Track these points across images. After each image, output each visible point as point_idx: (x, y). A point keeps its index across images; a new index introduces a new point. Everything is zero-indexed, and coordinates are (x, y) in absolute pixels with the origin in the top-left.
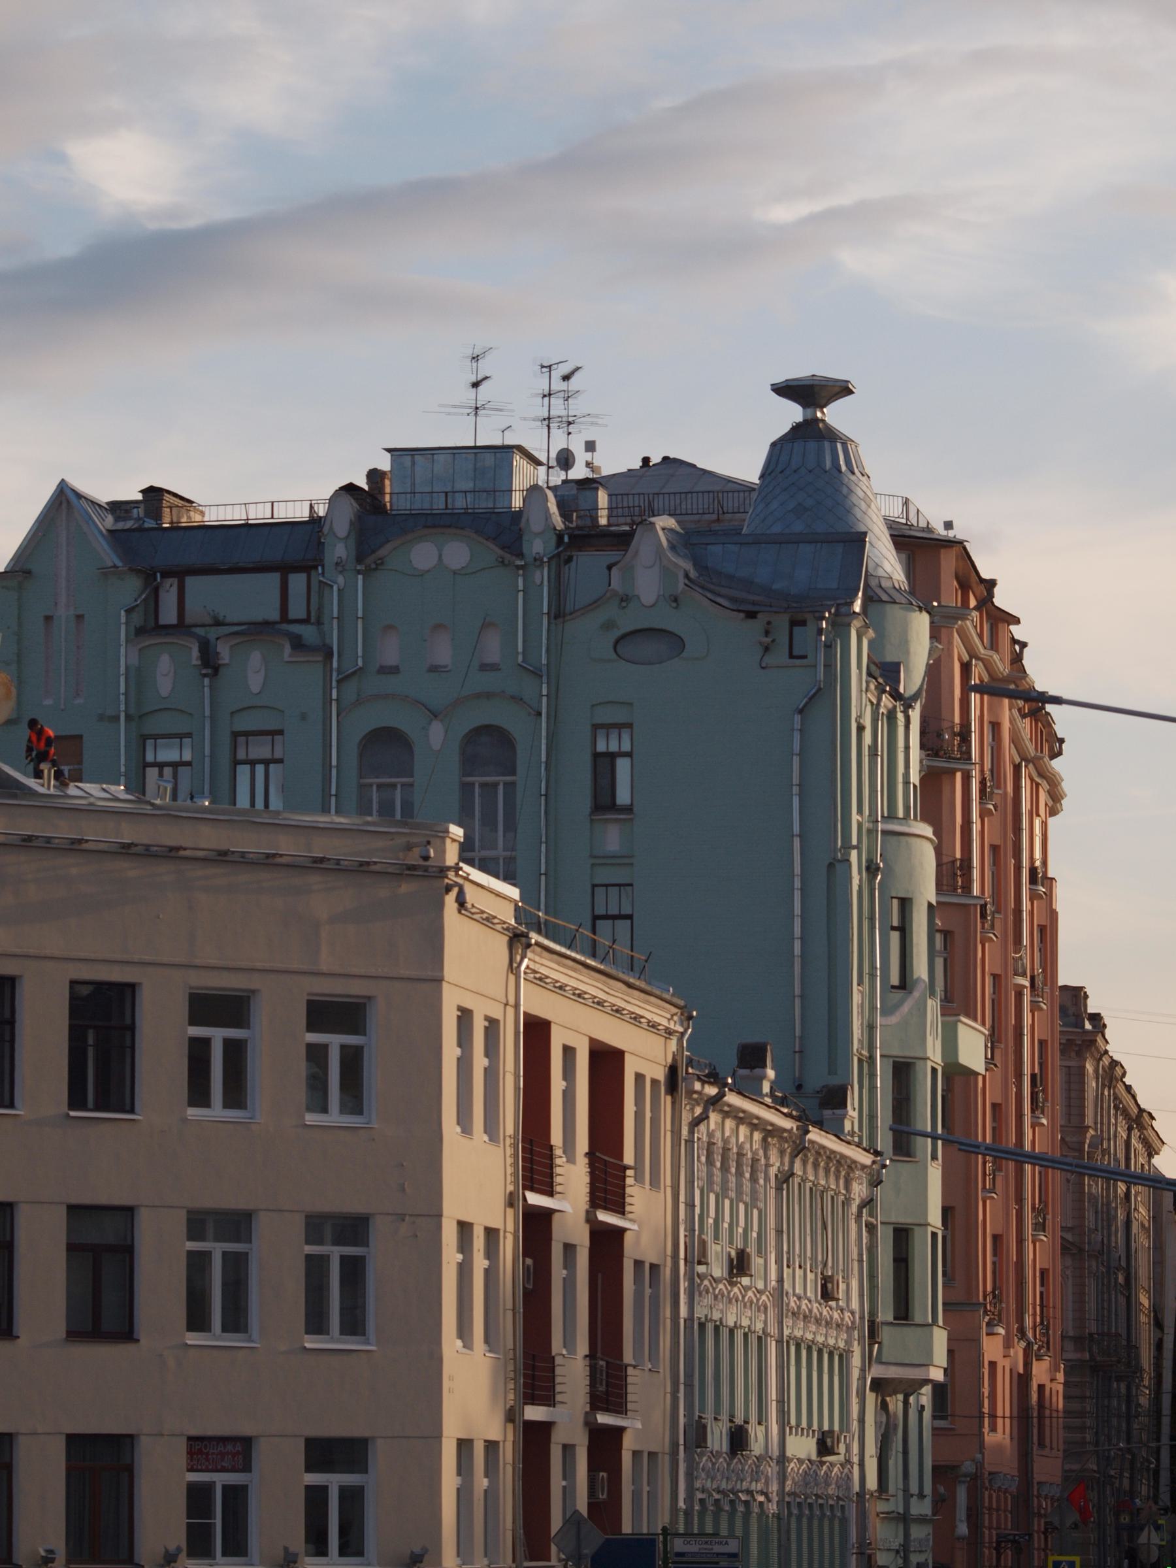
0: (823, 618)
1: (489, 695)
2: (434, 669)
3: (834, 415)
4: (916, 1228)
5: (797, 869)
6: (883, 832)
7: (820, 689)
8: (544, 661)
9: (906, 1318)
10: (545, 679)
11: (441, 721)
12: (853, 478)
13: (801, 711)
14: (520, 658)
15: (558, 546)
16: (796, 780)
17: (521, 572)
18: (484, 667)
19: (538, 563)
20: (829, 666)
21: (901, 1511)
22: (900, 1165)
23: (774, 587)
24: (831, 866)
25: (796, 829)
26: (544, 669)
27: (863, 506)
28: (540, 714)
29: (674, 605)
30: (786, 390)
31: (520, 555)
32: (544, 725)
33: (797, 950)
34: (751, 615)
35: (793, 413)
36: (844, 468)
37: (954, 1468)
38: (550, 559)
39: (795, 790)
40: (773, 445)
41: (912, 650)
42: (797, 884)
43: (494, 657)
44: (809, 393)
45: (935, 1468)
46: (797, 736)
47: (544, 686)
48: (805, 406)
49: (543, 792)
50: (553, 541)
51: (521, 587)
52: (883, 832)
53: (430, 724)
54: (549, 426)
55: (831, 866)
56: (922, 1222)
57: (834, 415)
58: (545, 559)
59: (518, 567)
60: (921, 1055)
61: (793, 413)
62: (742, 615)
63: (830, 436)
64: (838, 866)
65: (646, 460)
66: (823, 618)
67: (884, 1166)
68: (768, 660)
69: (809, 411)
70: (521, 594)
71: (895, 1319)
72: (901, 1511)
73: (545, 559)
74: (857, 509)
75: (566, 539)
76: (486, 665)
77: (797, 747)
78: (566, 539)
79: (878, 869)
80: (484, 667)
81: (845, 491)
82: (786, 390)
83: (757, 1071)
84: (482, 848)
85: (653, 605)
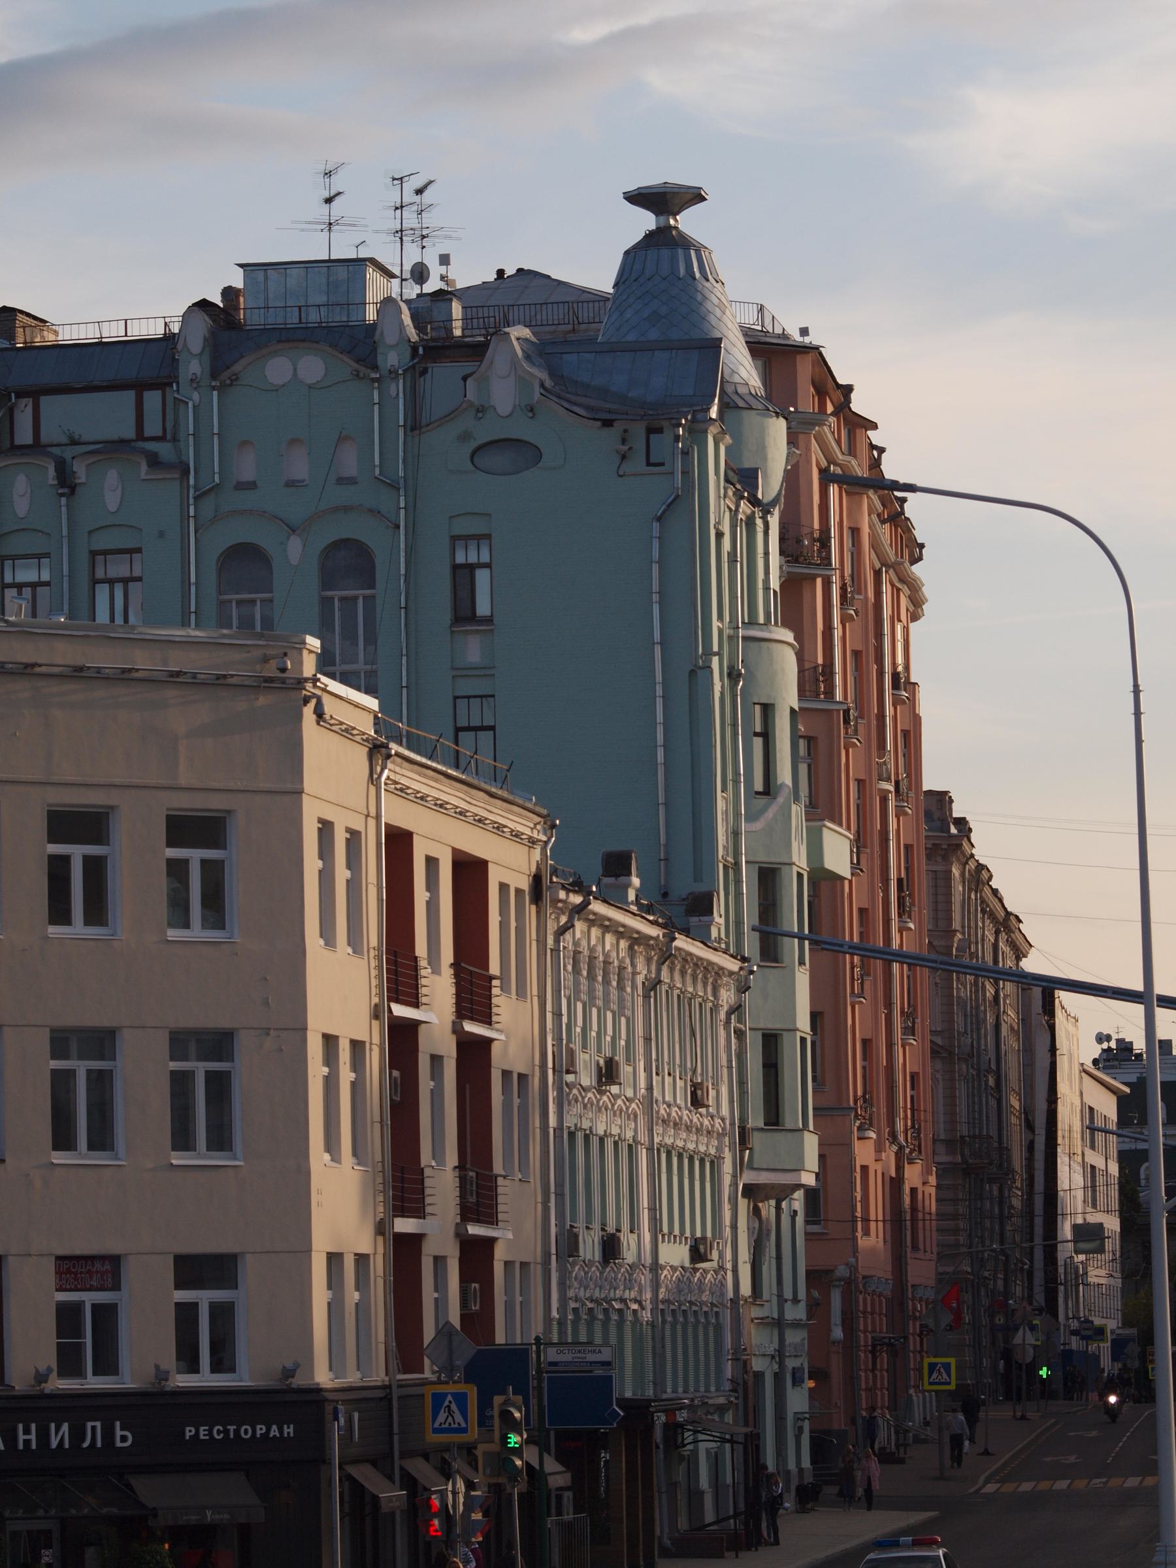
0: (680, 425)
1: (347, 509)
2: (291, 484)
3: (687, 222)
4: (784, 1033)
5: (659, 677)
8: (401, 474)
9: (777, 1124)
10: (402, 492)
12: (707, 284)
13: (659, 519)
16: (655, 588)
17: (376, 385)
19: (393, 376)
20: (687, 473)
21: (776, 1316)
22: (767, 970)
26: (402, 481)
27: (718, 312)
28: (398, 527)
29: (530, 414)
30: (639, 198)
31: (375, 368)
33: (660, 757)
34: (608, 423)
36: (698, 275)
39: (655, 597)
40: (627, 253)
41: (769, 456)
42: (659, 691)
44: (661, 200)
46: (656, 544)
47: (402, 499)
48: (657, 213)
49: (403, 605)
50: (408, 353)
53: (288, 539)
55: (692, 673)
57: (687, 222)
58: (400, 372)
59: (373, 380)
60: (786, 861)
62: (599, 423)
63: (684, 243)
65: (500, 273)
66: (680, 425)
67: (752, 972)
68: (626, 468)
69: (662, 218)
70: (376, 407)
71: (766, 1124)
72: (776, 1316)
73: (400, 372)
75: (421, 351)
77: (656, 555)
78: (421, 351)
79: (740, 675)
81: (699, 297)
82: (639, 198)
83: (622, 879)
84: (343, 662)
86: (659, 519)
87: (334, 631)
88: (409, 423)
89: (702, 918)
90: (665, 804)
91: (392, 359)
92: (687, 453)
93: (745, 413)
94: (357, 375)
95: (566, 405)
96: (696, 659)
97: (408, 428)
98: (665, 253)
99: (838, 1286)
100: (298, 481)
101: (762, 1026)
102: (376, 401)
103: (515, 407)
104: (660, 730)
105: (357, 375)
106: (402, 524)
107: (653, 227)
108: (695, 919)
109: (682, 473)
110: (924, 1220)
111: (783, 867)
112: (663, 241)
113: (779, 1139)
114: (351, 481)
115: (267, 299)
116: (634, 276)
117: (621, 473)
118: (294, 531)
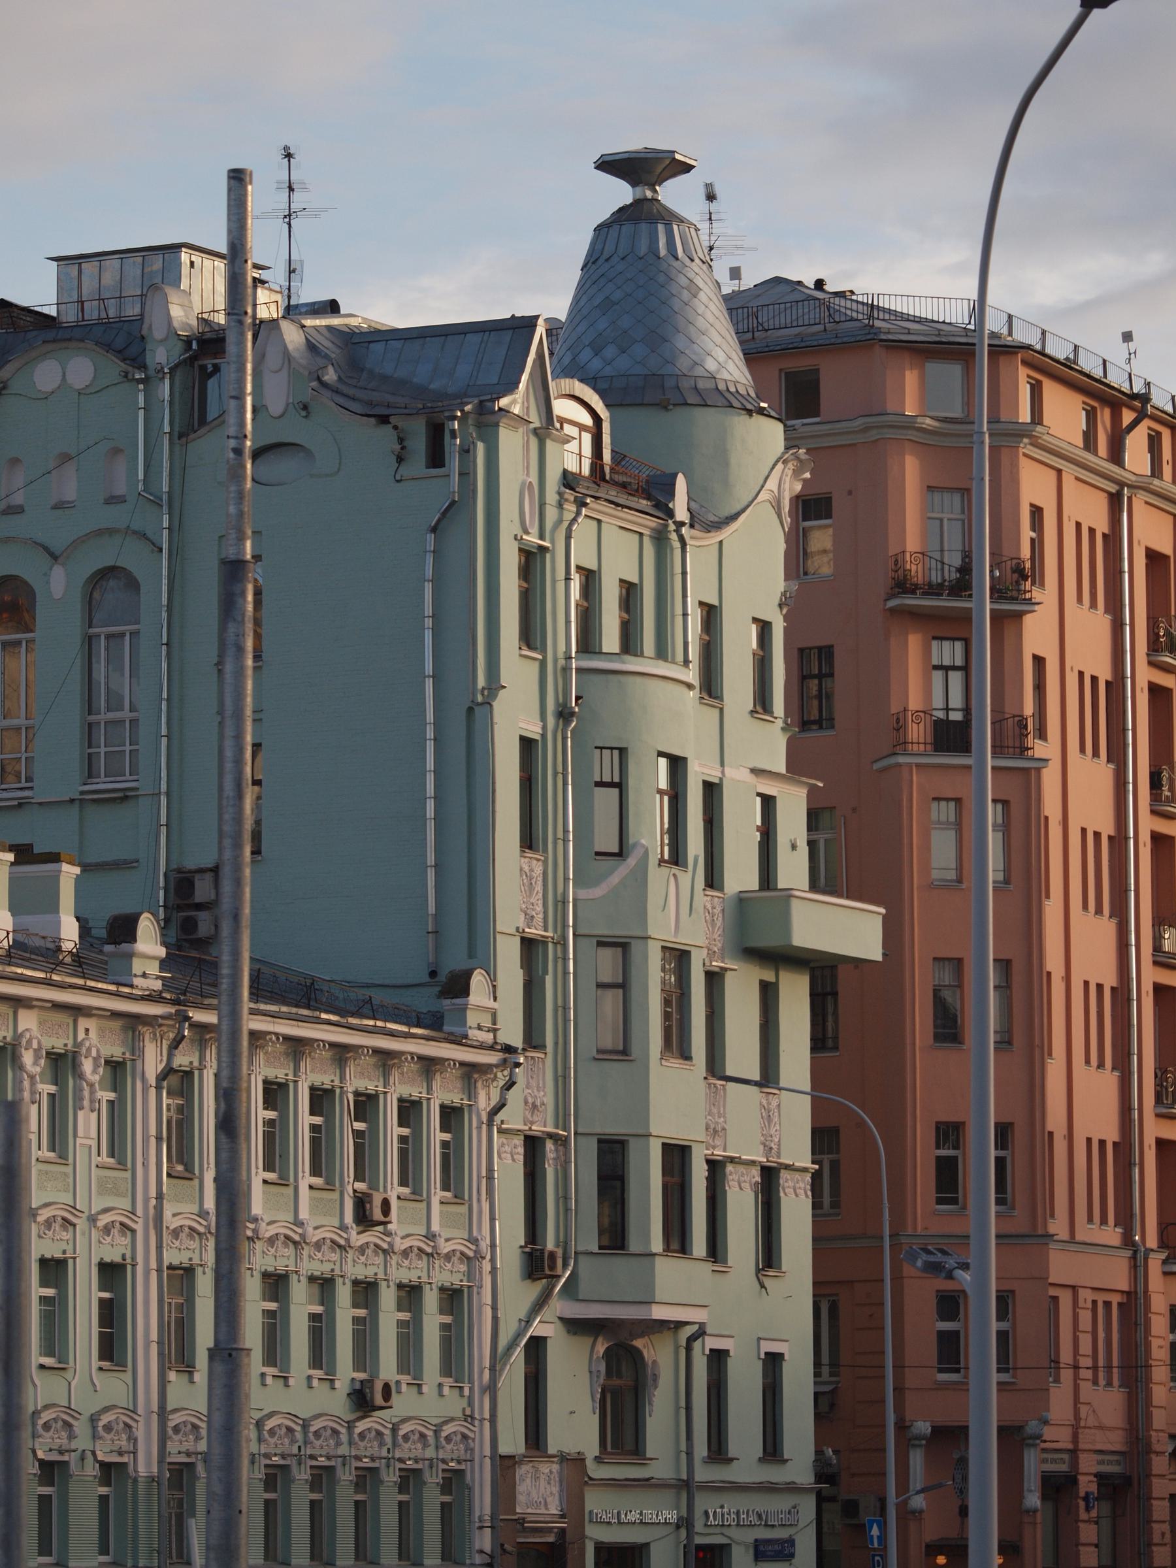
0: (455, 418)
1: (110, 532)
2: (59, 506)
3: (674, 194)
4: (631, 1140)
5: (430, 717)
6: (579, 670)
7: (453, 503)
8: (165, 489)
9: (622, 1247)
10: (165, 509)
11: (63, 565)
12: (676, 264)
13: (434, 530)
14: (141, 487)
15: (186, 351)
16: (428, 610)
17: (141, 386)
18: (113, 500)
19: (160, 375)
20: (467, 474)
21: (685, 1477)
22: (607, 1064)
23: (432, 386)
24: (470, 710)
25: (429, 669)
26: (165, 497)
27: (685, 295)
28: (161, 550)
29: (304, 413)
30: (608, 165)
31: (143, 367)
32: (165, 563)
33: (430, 811)
34: (384, 420)
35: (621, 193)
36: (663, 252)
37: (1020, 1428)
38: (173, 370)
39: (429, 623)
40: (599, 229)
41: (733, 461)
42: (430, 734)
43: (121, 489)
44: (640, 168)
45: (1000, 1429)
46: (430, 559)
47: (166, 517)
48: (634, 183)
49: (165, 640)
50: (180, 346)
51: (141, 404)
52: (579, 670)
53: (51, 569)
54: (289, 224)
55: (470, 710)
56: (641, 1132)
57: (674, 194)
58: (166, 370)
59: (139, 381)
60: (639, 933)
61: (621, 193)
62: (372, 420)
63: (669, 218)
64: (477, 709)
65: (819, 284)
66: (455, 418)
67: (518, 1065)
68: (405, 471)
69: (639, 189)
70: (141, 412)
71: (600, 1248)
72: (685, 1477)
73: (166, 370)
74: (676, 300)
75: (195, 346)
76: (113, 497)
77: (429, 573)
78: (195, 346)
79: (572, 714)
80: (113, 500)
81: (661, 278)
82: (608, 165)
83: (125, 947)
84: (109, 710)
85: (280, 417)
86: (434, 530)
87: (123, 675)
88: (177, 429)
89: (455, 1001)
90: (436, 866)
91: (161, 356)
92: (468, 451)
93: (699, 412)
94: (126, 376)
95: (341, 400)
96: (474, 695)
97: (176, 434)
98: (644, 227)
99: (919, 1446)
100: (69, 502)
101: (599, 1130)
102: (142, 404)
103: (288, 405)
104: (430, 779)
105: (126, 376)
106: (165, 546)
107: (629, 200)
108: (448, 1001)
109: (460, 474)
110: (1076, 1367)
111: (633, 942)
112: (641, 216)
113: (619, 1265)
114: (121, 500)
115: (80, 294)
116: (606, 255)
117: (398, 478)
118: (55, 557)
